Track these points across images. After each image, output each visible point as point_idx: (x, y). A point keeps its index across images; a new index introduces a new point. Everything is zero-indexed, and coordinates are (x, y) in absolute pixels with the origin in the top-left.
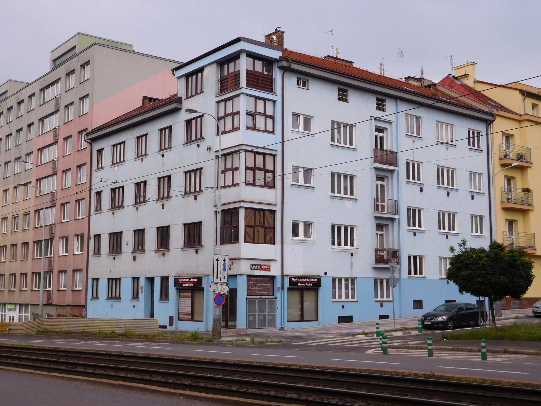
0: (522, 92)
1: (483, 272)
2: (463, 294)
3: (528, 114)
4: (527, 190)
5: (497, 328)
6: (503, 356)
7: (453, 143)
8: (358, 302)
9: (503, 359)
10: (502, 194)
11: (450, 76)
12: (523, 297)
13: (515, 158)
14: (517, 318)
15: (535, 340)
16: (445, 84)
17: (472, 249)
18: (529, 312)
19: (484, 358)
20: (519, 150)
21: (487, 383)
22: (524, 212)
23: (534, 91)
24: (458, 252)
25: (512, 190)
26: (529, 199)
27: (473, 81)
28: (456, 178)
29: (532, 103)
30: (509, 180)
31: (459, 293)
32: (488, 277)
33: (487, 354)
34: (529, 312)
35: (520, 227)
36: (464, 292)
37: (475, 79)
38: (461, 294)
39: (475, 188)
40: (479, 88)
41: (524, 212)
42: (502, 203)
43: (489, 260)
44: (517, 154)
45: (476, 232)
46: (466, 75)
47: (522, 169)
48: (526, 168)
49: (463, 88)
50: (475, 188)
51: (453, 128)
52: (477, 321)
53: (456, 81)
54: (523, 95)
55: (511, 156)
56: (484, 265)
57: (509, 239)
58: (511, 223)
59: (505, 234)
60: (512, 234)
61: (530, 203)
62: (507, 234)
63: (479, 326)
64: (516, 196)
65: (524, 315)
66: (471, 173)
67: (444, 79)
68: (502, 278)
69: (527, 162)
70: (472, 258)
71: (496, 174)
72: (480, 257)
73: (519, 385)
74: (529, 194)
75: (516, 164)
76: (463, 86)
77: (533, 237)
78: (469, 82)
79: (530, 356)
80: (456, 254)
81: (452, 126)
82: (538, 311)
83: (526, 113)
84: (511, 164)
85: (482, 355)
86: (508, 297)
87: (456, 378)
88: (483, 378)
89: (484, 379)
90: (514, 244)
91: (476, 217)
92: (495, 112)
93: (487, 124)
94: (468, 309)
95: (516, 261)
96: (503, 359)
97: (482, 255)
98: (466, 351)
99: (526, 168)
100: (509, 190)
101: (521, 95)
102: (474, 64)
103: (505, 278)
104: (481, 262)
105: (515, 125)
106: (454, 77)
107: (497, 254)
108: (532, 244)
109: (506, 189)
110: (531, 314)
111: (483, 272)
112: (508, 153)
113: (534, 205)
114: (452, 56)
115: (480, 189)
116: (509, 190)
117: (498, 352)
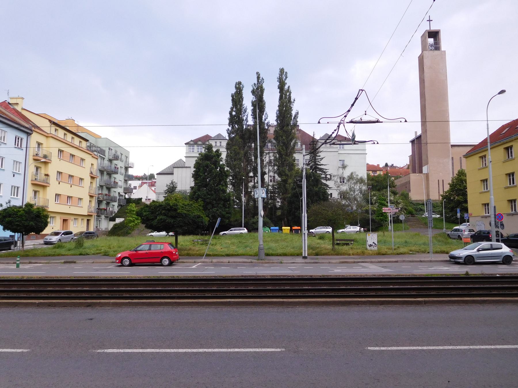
0: (50, 121)
1: (20, 219)
2: (5, 231)
3: (52, 134)
4: (47, 175)
5: (24, 251)
6: (29, 265)
7: (22, 148)
8: (443, 180)
9: (29, 267)
10: (32, 176)
11: (6, 101)
12: (42, 233)
13: (42, 157)
14: (34, 245)
15: (46, 256)
16: (2, 106)
17: (14, 206)
18: (42, 241)
19: (18, 266)
20: (45, 153)
21: (25, 278)
22: (44, 187)
23: (56, 122)
24: (5, 207)
25: (39, 174)
26: (48, 180)
27: (21, 108)
28: (4, 163)
29: (72, 137)
30: (37, 168)
31: (3, 230)
32: (23, 222)
33: (20, 264)
34: (42, 241)
35: (41, 195)
36: (6, 230)
37: (22, 107)
38: (4, 231)
39: (16, 170)
40: (24, 113)
41: (44, 187)
42: (32, 180)
43: (24, 213)
44: (44, 155)
45: (14, 196)
46: (17, 104)
47: (46, 163)
48: (48, 163)
49: (14, 111)
50: (16, 170)
51: (6, 133)
52: (10, 247)
53: (10, 106)
54: (51, 123)
55: (40, 155)
56: (21, 215)
57: (34, 201)
58: (35, 192)
59: (32, 198)
60: (36, 199)
61: (48, 182)
62: (32, 198)
63: (11, 250)
64: (40, 177)
65: (38, 243)
66: (14, 161)
67: (2, 102)
68: (31, 223)
69: (49, 160)
70: (14, 211)
71: (30, 165)
72: (19, 210)
73: (43, 278)
74: (48, 178)
75: (43, 160)
76: (14, 110)
77: (48, 201)
78: (19, 108)
79: (44, 264)
80: (4, 208)
81: (5, 132)
82: (47, 241)
83: (51, 133)
84: (40, 160)
85: (17, 265)
86: (32, 233)
87: (6, 277)
88: (22, 276)
89: (23, 277)
90: (36, 204)
91: (15, 187)
92: (33, 129)
93: (28, 135)
94: (5, 240)
95: (41, 214)
96: (29, 267)
97: (20, 209)
98: (5, 264)
99: (48, 163)
100: (37, 174)
101: (49, 122)
102: (23, 98)
103: (33, 223)
104: (19, 213)
105: (45, 138)
106: (9, 103)
107: (29, 210)
108: (47, 205)
109: (35, 173)
110: (43, 243)
111: (20, 219)
112: (38, 153)
113: (50, 183)
114: (9, 90)
115: (19, 172)
116: (37, 174)
117: (25, 263)
